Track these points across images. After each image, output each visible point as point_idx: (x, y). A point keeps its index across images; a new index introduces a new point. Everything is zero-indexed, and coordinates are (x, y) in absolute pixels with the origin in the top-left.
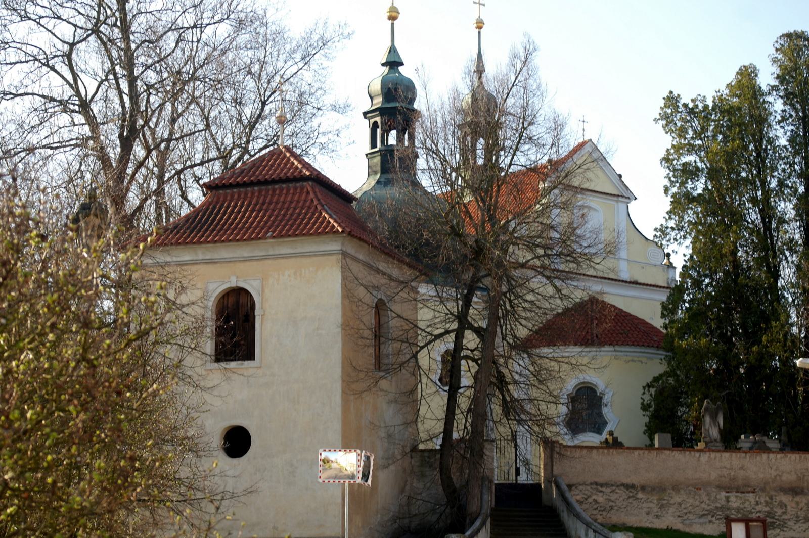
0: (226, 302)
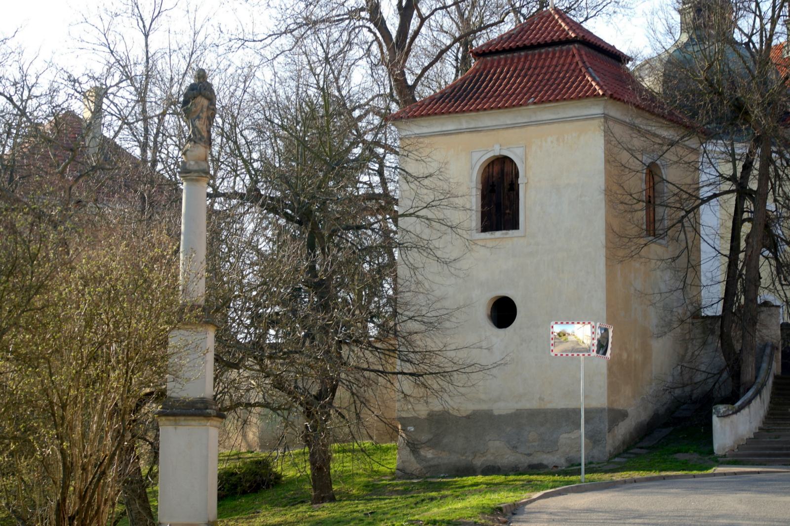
0: (491, 170)
